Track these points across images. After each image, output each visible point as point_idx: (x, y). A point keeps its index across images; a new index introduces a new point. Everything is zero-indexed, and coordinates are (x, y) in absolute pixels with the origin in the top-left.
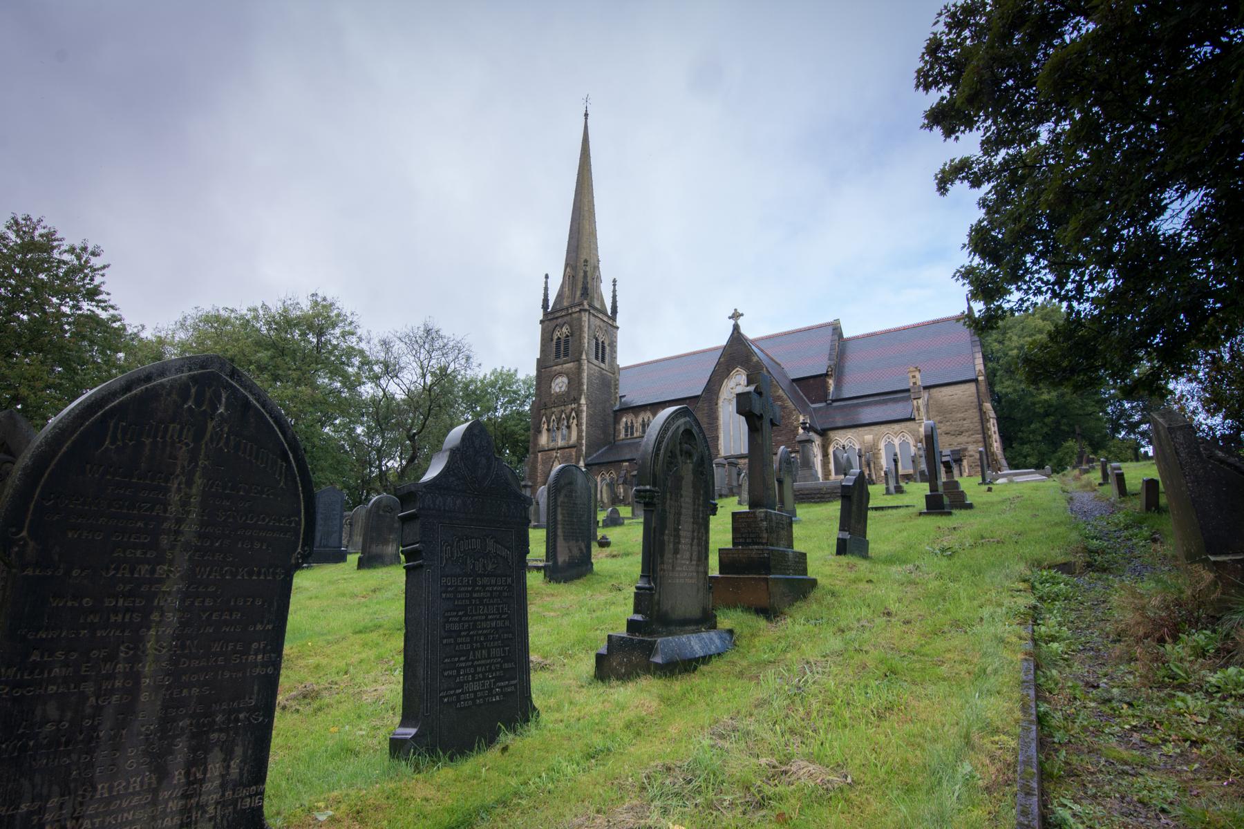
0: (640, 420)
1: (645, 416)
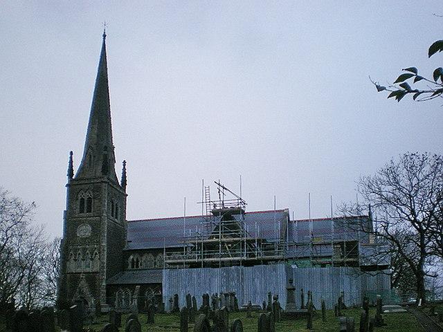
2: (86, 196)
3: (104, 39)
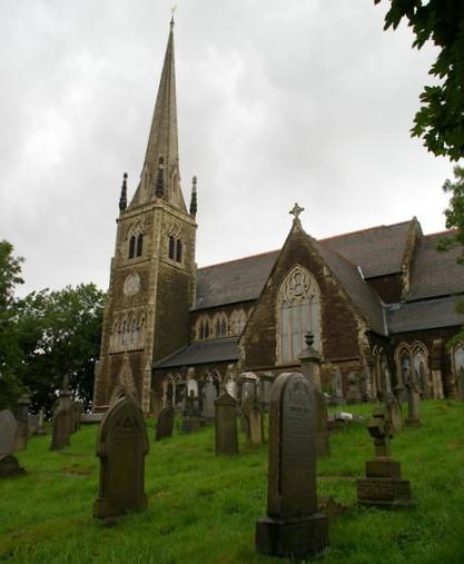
0: (215, 321)
1: (221, 317)
2: (136, 232)
3: (172, 27)
